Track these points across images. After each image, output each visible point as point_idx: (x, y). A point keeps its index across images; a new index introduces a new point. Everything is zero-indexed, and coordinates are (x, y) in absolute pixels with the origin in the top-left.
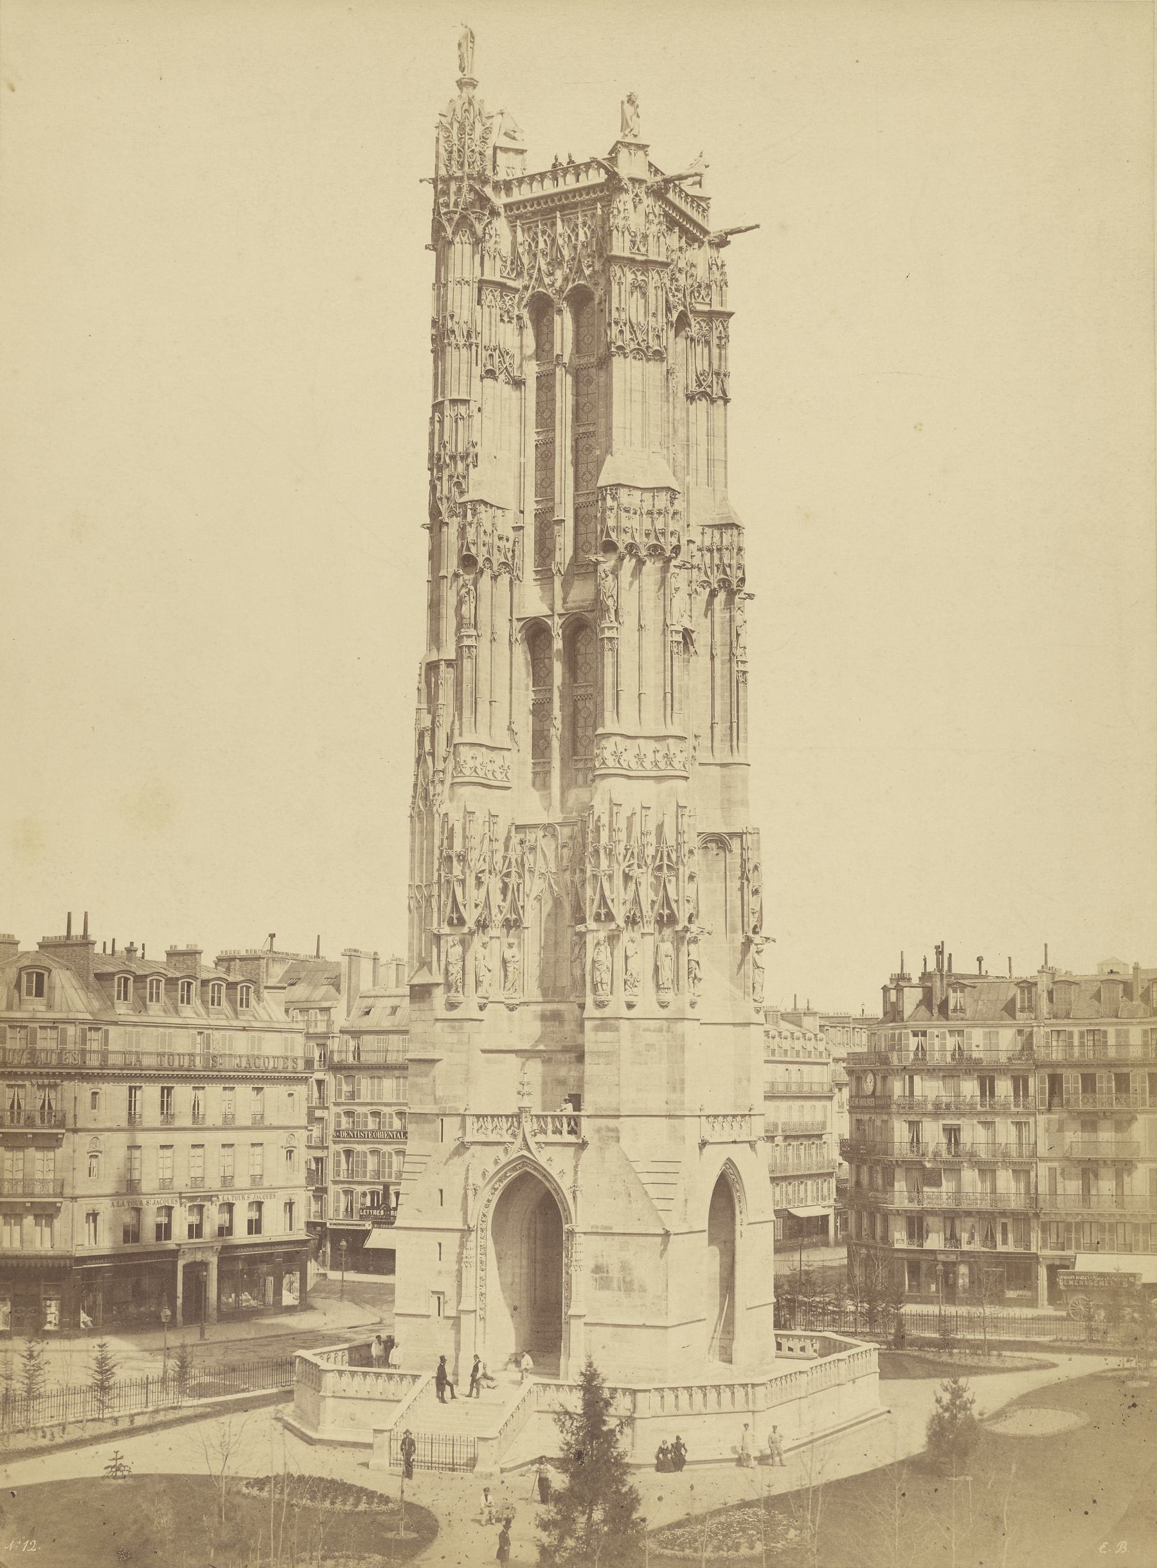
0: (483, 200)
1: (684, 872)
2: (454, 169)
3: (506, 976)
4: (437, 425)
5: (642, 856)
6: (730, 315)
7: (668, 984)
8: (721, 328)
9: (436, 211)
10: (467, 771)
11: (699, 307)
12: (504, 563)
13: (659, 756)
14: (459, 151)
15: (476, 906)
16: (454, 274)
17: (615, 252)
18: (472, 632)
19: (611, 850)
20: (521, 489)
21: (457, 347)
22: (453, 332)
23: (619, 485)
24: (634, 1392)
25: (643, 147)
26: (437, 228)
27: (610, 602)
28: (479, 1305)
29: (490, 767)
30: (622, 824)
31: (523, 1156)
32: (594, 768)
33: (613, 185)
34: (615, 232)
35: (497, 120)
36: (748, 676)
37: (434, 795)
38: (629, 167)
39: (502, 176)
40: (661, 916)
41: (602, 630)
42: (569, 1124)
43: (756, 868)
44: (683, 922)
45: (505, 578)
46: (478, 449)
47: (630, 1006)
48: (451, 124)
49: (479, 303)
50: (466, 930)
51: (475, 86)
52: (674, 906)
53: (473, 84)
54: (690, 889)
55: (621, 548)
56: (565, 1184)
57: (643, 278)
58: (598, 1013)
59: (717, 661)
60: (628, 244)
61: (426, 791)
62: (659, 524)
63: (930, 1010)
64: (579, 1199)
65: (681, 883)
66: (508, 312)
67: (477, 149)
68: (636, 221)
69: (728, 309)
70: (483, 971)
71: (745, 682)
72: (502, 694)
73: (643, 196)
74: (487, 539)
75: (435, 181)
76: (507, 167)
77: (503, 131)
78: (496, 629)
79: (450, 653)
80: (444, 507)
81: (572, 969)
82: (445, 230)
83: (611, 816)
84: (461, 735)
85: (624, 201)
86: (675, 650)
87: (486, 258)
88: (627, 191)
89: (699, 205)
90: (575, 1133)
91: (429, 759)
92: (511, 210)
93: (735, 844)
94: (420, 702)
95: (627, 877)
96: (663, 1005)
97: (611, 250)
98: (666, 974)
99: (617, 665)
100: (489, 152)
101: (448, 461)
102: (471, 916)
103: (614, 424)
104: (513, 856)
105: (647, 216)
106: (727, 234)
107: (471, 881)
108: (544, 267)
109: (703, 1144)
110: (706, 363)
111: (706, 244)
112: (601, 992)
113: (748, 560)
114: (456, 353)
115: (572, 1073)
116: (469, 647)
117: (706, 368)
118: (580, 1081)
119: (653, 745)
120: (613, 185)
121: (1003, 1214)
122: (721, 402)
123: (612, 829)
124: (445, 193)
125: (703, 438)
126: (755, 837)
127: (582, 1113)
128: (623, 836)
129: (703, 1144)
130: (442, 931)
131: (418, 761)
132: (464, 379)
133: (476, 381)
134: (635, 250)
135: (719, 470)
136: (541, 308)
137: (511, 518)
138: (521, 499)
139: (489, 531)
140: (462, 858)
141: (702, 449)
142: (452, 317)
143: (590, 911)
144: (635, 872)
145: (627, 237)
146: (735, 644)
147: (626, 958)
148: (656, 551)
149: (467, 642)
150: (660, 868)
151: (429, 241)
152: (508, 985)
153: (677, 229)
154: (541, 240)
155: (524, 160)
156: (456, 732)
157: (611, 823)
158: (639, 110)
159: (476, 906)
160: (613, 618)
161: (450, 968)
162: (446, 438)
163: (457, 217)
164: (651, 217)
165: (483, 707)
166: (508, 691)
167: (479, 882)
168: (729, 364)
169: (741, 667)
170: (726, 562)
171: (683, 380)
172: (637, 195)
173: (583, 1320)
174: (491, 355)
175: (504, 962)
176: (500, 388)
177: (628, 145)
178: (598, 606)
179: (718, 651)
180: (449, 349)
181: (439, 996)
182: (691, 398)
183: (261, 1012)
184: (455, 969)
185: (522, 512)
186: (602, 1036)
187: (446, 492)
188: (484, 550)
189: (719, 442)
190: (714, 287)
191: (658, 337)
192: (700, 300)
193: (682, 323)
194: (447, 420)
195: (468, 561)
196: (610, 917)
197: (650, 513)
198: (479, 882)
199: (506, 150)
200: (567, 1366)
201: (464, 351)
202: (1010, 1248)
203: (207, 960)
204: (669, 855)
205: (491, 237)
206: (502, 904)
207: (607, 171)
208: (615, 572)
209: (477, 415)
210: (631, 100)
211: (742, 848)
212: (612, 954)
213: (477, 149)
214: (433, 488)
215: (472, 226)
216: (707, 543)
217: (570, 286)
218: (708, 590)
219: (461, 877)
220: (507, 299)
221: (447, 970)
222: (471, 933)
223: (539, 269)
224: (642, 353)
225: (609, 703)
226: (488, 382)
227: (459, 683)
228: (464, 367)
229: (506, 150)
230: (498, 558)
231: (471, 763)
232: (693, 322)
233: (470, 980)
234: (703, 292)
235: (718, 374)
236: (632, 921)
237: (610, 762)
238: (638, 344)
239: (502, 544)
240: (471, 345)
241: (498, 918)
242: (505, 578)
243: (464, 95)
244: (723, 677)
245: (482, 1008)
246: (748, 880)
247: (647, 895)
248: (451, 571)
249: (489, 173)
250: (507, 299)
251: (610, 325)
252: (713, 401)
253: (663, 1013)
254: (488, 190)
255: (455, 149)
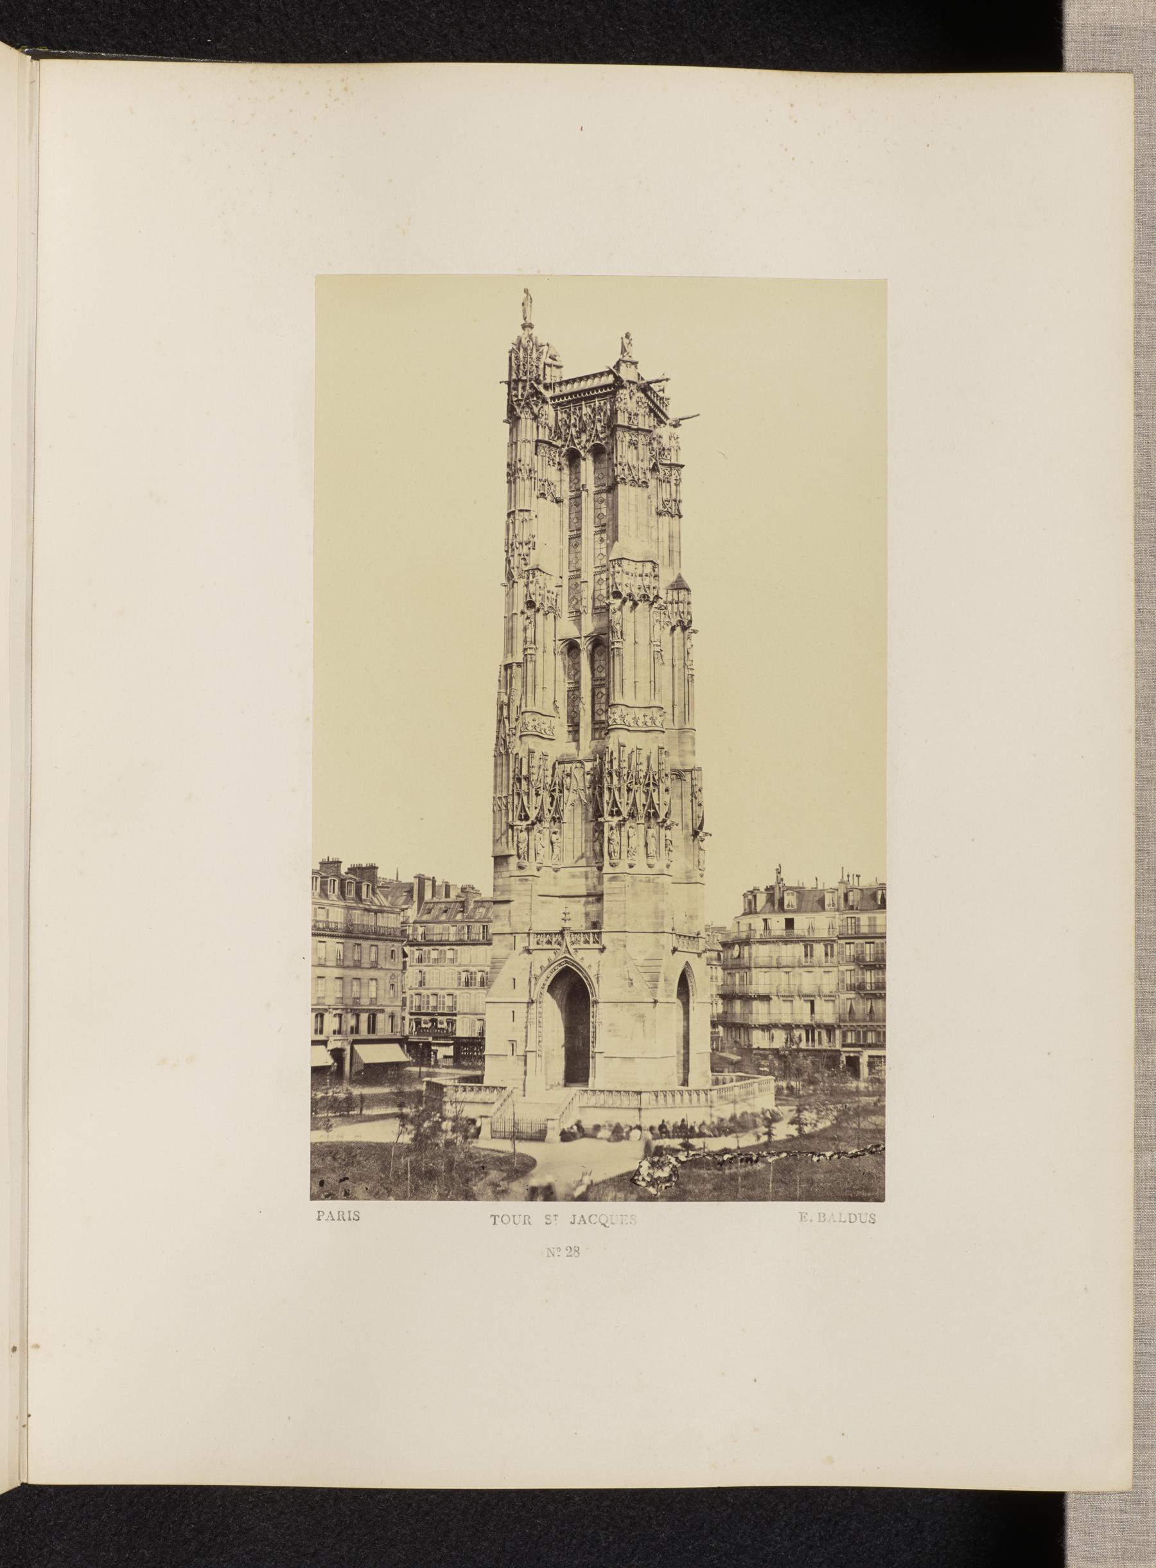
0: (537, 393)
1: (662, 787)
2: (521, 375)
3: (553, 851)
4: (511, 525)
5: (637, 778)
6: (682, 466)
7: (653, 854)
8: (677, 474)
9: (510, 401)
10: (530, 728)
11: (664, 462)
12: (551, 607)
13: (647, 719)
14: (524, 365)
15: (536, 808)
16: (522, 436)
17: (620, 422)
18: (533, 646)
19: (619, 773)
20: (561, 564)
21: (523, 479)
22: (521, 470)
23: (623, 558)
24: (640, 1093)
25: (635, 363)
26: (511, 410)
27: (618, 627)
28: (538, 1047)
29: (543, 726)
30: (625, 757)
31: (566, 957)
32: (609, 725)
33: (618, 384)
34: (619, 412)
35: (545, 349)
36: (695, 678)
37: (509, 743)
38: (626, 373)
39: (548, 381)
40: (649, 813)
41: (613, 643)
42: (594, 937)
43: (700, 790)
44: (662, 816)
45: (551, 616)
46: (535, 539)
47: (631, 866)
48: (519, 349)
49: (536, 454)
50: (529, 822)
51: (532, 328)
52: (657, 807)
53: (531, 326)
54: (666, 798)
55: (624, 595)
56: (592, 973)
57: (636, 438)
58: (611, 870)
59: (676, 669)
60: (627, 419)
61: (505, 741)
62: (647, 582)
63: (773, 904)
64: (600, 982)
65: (661, 795)
66: (553, 460)
67: (535, 364)
68: (631, 406)
69: (680, 463)
70: (540, 847)
71: (692, 681)
72: (550, 685)
73: (635, 391)
74: (542, 592)
75: (509, 383)
76: (551, 376)
77: (548, 355)
78: (547, 645)
79: (519, 658)
80: (515, 573)
81: (594, 846)
82: (515, 410)
83: (619, 753)
84: (526, 706)
85: (623, 393)
86: (656, 657)
87: (540, 427)
88: (626, 388)
89: (663, 402)
90: (598, 942)
91: (506, 721)
92: (554, 401)
93: (688, 777)
94: (500, 688)
95: (629, 790)
96: (650, 866)
97: (617, 422)
98: (652, 848)
99: (622, 664)
100: (541, 366)
101: (518, 546)
102: (533, 814)
103: (619, 523)
104: (557, 780)
105: (638, 403)
106: (680, 419)
107: (533, 792)
108: (574, 434)
109: (675, 950)
110: (668, 494)
111: (668, 425)
112: (614, 857)
113: (694, 609)
114: (522, 483)
115: (594, 909)
116: (531, 654)
117: (668, 497)
118: (600, 914)
119: (644, 711)
120: (618, 384)
121: (819, 1026)
122: (677, 517)
123: (620, 761)
124: (516, 389)
125: (666, 539)
126: (700, 772)
127: (602, 930)
128: (625, 764)
129: (675, 950)
130: (515, 824)
131: (499, 721)
132: (527, 498)
133: (534, 499)
134: (631, 423)
135: (676, 557)
136: (573, 458)
137: (555, 581)
138: (561, 570)
139: (542, 587)
140: (527, 779)
141: (666, 545)
142: (520, 461)
143: (607, 809)
144: (635, 787)
145: (627, 415)
146: (686, 659)
147: (629, 837)
148: (645, 597)
149: (529, 651)
150: (648, 785)
151: (506, 418)
152: (554, 856)
153: (652, 415)
154: (572, 418)
155: (561, 372)
156: (523, 705)
157: (619, 757)
158: (632, 342)
159: (536, 808)
160: (620, 636)
161: (520, 845)
162: (516, 532)
163: (523, 403)
164: (640, 404)
165: (539, 690)
166: (553, 682)
167: (537, 794)
168: (682, 495)
169: (690, 672)
170: (681, 610)
171: (656, 503)
172: (631, 391)
173: (604, 1055)
174: (543, 485)
175: (552, 843)
176: (547, 504)
177: (625, 362)
178: (610, 628)
179: (676, 663)
180: (518, 480)
181: (514, 861)
182: (659, 514)
183: (375, 900)
184: (523, 846)
185: (561, 577)
186: (614, 884)
187: (516, 564)
188: (539, 598)
189: (676, 541)
190: (672, 450)
191: (645, 473)
192: (664, 457)
193: (654, 469)
194: (517, 522)
195: (530, 604)
196: (619, 813)
197: (641, 575)
198: (537, 794)
199: (550, 366)
200: (594, 1083)
201: (527, 482)
202: (825, 1045)
203: (344, 869)
204: (654, 777)
205: (543, 415)
206: (550, 808)
207: (615, 376)
208: (620, 609)
209: (535, 519)
210: (627, 336)
211: (692, 779)
212: (620, 835)
213: (535, 364)
214: (508, 561)
215: (532, 409)
216: (670, 599)
217: (592, 444)
218: (670, 627)
219: (527, 791)
220: (552, 452)
221: (518, 847)
222: (533, 824)
223: (572, 435)
224: (635, 482)
225: (617, 688)
226: (542, 500)
227: (524, 678)
228: (527, 491)
229: (550, 366)
230: (547, 604)
231: (532, 723)
232: (661, 471)
233: (532, 852)
234: (666, 453)
235: (675, 501)
236: (632, 815)
237: (619, 721)
238: (633, 477)
239: (550, 595)
240: (531, 478)
241: (548, 816)
242: (551, 616)
243: (526, 333)
244: (679, 678)
245: (538, 870)
246: (696, 798)
247: (641, 799)
248: (519, 610)
249: (541, 378)
250: (552, 452)
251: (616, 465)
252: (672, 516)
253: (649, 871)
254: (541, 388)
255: (521, 363)
